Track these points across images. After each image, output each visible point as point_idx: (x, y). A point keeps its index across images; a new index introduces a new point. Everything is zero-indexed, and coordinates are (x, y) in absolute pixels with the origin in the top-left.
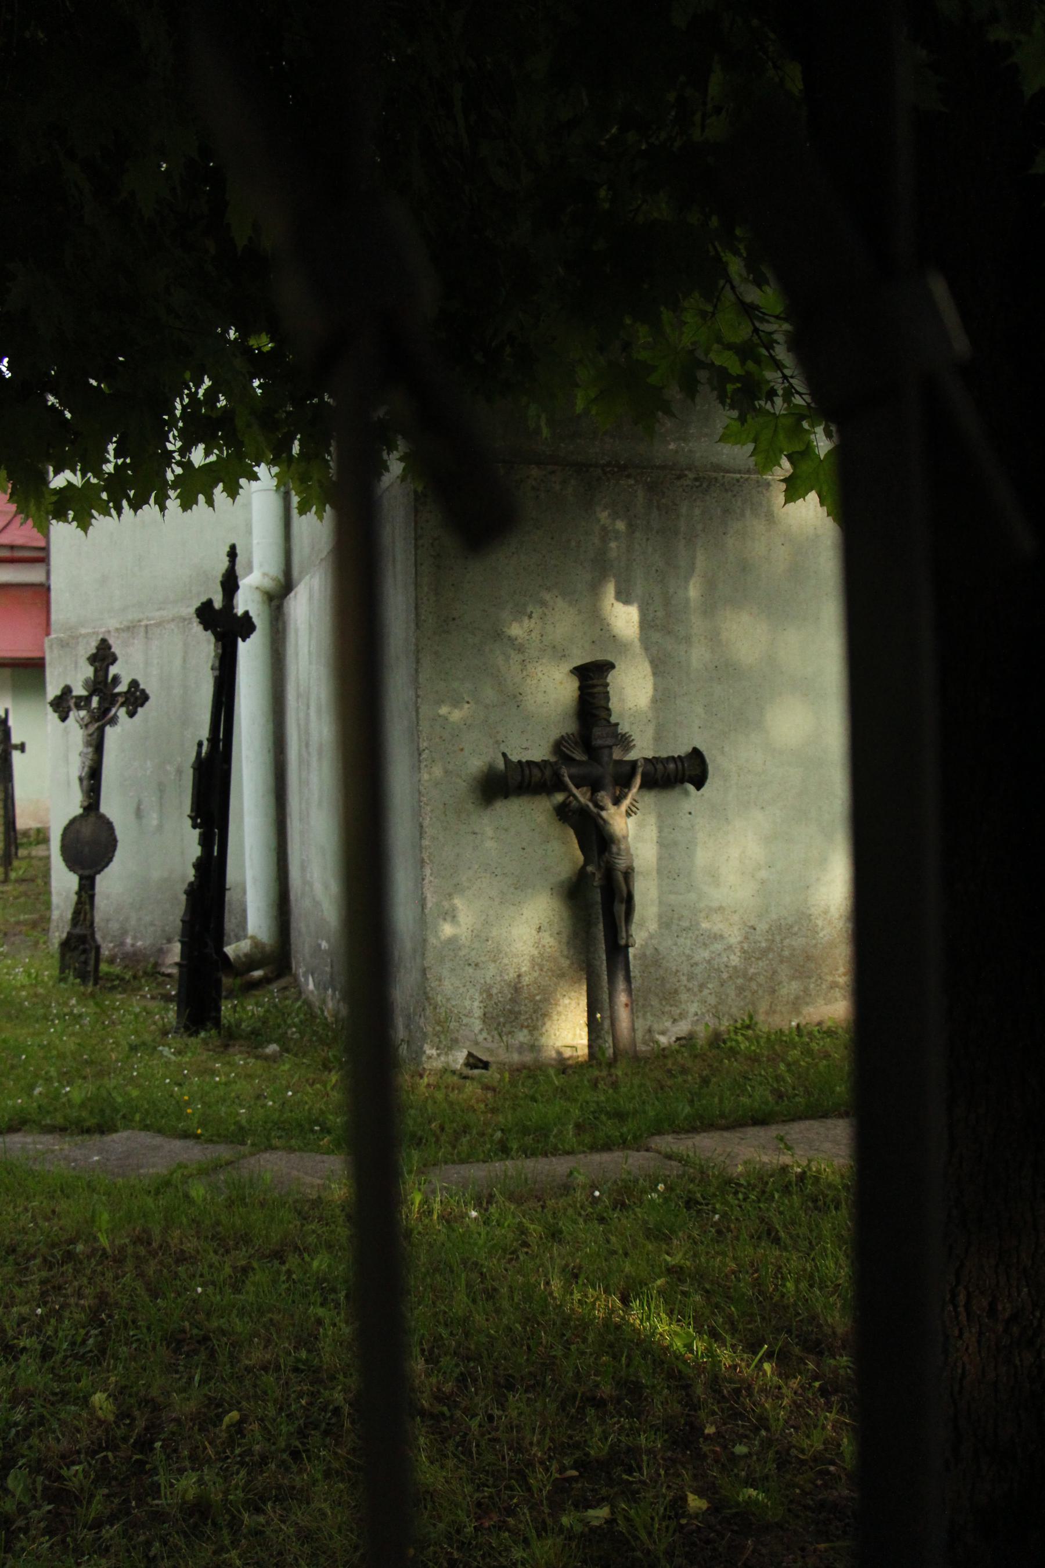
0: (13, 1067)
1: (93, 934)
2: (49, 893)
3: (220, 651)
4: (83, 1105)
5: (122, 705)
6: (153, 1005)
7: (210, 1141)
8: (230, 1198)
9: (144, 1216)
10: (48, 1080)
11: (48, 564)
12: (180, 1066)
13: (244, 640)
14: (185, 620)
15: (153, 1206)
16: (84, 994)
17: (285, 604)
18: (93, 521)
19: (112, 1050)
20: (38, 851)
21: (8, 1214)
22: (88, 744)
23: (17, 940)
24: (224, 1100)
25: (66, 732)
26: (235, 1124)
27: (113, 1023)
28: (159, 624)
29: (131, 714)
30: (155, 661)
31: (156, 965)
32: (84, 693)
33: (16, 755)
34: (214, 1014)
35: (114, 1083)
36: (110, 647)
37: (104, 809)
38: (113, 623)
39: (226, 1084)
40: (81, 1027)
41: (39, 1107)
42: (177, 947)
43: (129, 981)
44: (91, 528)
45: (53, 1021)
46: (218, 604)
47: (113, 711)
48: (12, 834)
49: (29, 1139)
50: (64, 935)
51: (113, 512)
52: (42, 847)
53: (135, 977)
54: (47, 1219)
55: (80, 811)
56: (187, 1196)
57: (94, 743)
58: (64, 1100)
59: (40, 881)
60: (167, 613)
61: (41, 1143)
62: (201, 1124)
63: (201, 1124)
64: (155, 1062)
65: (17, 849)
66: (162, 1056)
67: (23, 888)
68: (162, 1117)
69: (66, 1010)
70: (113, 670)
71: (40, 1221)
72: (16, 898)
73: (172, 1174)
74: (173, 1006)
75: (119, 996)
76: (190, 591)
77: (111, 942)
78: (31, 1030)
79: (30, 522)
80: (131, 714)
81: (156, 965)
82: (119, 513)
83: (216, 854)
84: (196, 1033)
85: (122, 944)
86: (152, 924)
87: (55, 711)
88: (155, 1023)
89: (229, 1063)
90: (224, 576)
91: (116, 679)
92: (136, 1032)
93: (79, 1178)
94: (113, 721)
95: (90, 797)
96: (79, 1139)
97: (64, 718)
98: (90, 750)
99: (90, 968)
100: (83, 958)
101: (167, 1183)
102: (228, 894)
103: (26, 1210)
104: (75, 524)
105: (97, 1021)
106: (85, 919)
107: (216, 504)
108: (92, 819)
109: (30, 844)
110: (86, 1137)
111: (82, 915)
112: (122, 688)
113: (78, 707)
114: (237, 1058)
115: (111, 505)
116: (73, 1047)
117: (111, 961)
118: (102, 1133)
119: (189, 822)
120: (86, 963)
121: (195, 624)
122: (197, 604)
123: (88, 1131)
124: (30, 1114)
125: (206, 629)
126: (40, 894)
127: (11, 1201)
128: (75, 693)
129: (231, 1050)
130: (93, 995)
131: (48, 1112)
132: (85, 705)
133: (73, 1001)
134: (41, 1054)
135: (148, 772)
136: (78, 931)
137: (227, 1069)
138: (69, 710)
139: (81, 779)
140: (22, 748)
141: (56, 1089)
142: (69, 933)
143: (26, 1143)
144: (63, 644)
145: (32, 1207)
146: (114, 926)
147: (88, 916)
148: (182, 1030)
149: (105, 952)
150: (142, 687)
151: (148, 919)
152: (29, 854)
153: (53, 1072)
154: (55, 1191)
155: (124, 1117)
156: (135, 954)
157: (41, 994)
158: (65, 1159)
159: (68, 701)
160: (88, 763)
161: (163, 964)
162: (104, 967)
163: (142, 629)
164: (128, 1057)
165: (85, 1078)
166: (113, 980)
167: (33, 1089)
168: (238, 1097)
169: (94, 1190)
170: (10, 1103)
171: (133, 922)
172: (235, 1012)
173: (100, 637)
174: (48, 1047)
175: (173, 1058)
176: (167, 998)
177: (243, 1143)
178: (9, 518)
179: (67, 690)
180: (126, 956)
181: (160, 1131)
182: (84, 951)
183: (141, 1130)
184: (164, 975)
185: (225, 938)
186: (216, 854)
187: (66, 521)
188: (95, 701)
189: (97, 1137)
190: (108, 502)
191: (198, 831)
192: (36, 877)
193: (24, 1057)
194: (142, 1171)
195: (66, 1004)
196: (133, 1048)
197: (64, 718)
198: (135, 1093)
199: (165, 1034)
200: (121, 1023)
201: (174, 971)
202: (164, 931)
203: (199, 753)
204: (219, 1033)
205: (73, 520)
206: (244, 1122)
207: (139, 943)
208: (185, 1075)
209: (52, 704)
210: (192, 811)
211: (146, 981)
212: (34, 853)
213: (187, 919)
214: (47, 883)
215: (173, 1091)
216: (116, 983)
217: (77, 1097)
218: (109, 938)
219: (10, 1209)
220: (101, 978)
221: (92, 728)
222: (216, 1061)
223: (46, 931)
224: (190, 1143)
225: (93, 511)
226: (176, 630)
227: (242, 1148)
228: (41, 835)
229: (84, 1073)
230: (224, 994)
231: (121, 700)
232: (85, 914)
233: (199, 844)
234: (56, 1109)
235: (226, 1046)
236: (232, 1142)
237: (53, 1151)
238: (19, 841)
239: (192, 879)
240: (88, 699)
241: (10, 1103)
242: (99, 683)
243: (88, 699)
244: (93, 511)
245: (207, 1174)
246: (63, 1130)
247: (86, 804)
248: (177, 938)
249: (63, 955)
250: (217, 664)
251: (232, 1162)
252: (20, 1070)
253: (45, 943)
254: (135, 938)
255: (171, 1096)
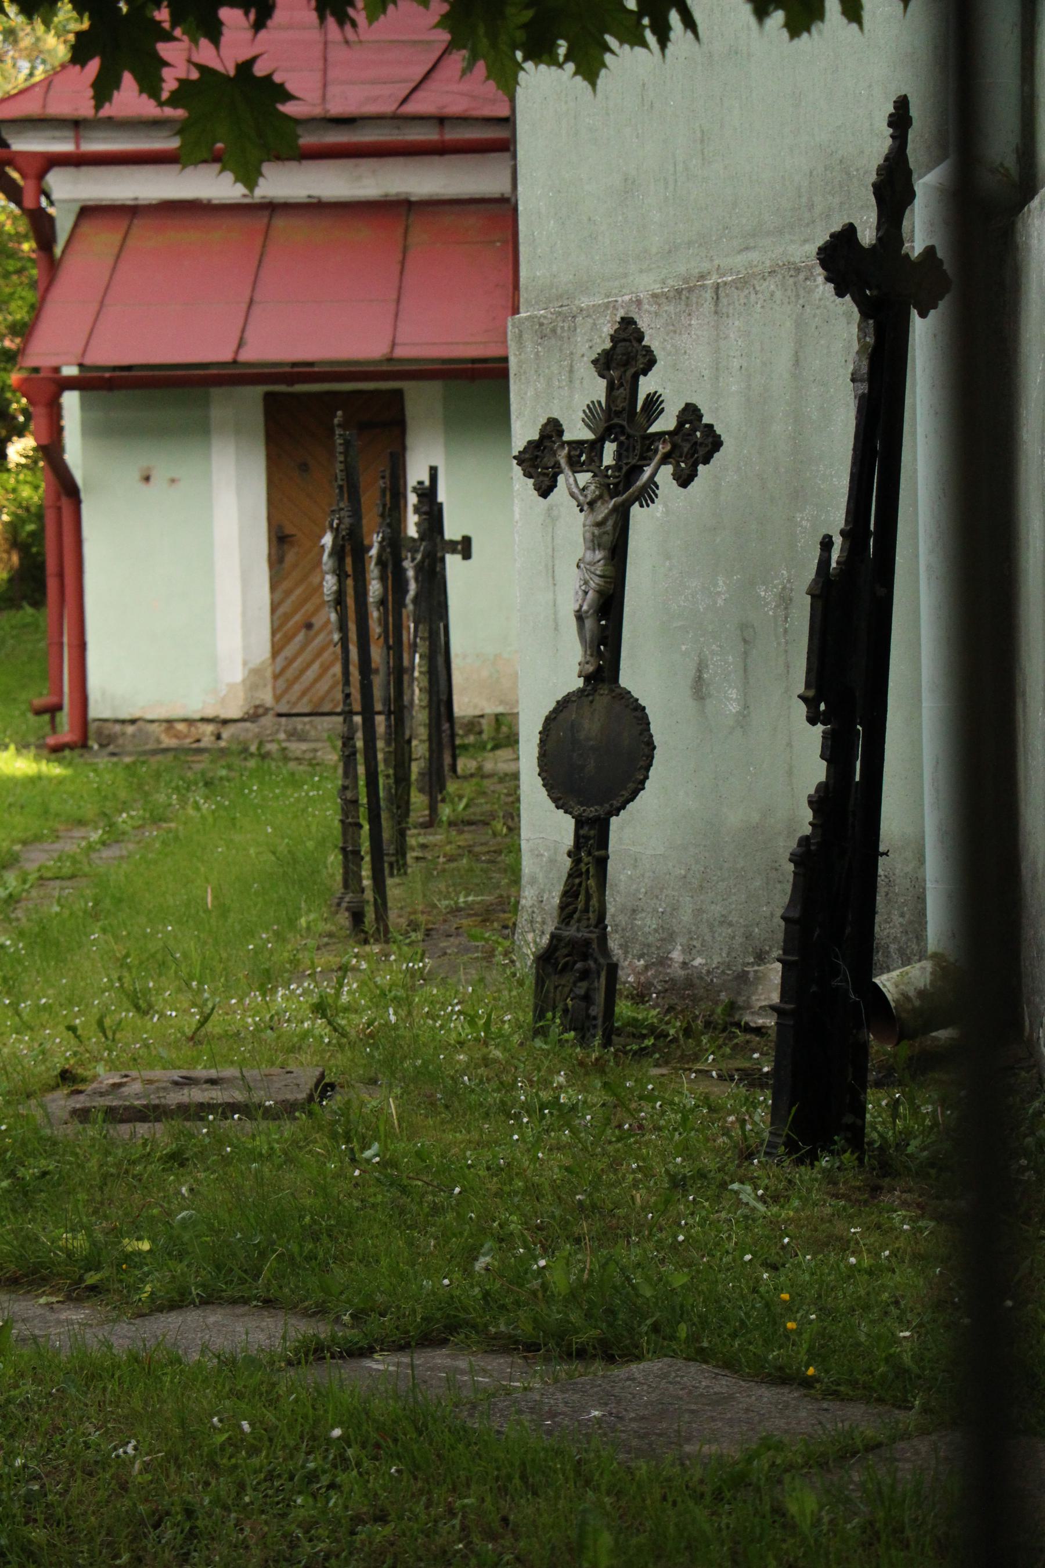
0: (436, 1210)
1: (603, 938)
2: (516, 850)
3: (870, 340)
4: (573, 1297)
5: (665, 460)
6: (727, 1093)
7: (833, 1394)
8: (871, 1523)
9: (688, 1547)
10: (504, 1239)
11: (514, 157)
12: (773, 1223)
13: (923, 315)
14: (798, 270)
15: (706, 1527)
16: (581, 1064)
17: (1019, 225)
18: (608, 57)
19: (635, 1184)
20: (495, 762)
21: (416, 1518)
22: (594, 543)
23: (450, 945)
24: (867, 1308)
25: (551, 517)
26: (887, 1360)
27: (641, 1127)
28: (742, 283)
29: (684, 480)
30: (736, 363)
31: (732, 1007)
32: (588, 435)
33: (453, 562)
34: (849, 1119)
35: (635, 1255)
36: (640, 336)
37: (625, 680)
38: (647, 283)
39: (870, 1272)
40: (574, 1132)
41: (486, 1295)
42: (775, 972)
43: (675, 1040)
44: (603, 72)
45: (517, 1117)
46: (867, 236)
47: (648, 471)
48: (446, 726)
49: (462, 1364)
50: (545, 940)
51: (649, 36)
52: (504, 753)
53: (688, 1032)
54: (491, 1536)
55: (580, 683)
56: (779, 1511)
57: (607, 539)
58: (536, 1284)
59: (499, 826)
60: (759, 258)
61: (485, 1372)
62: (813, 1357)
63: (813, 1357)
64: (723, 1215)
65: (454, 758)
66: (739, 1203)
67: (465, 839)
68: (734, 1335)
69: (545, 1095)
70: (647, 385)
71: (476, 1539)
72: (451, 859)
73: (749, 1460)
74: (764, 1097)
75: (655, 1071)
76: (811, 207)
77: (641, 956)
78: (475, 1136)
79: (481, 66)
80: (684, 480)
81: (732, 1007)
82: (663, 40)
83: (857, 779)
84: (813, 1158)
85: (663, 961)
86: (724, 921)
87: (528, 475)
88: (726, 1132)
89: (878, 1226)
90: (880, 170)
91: (654, 404)
92: (686, 1150)
93: (558, 1453)
94: (647, 494)
95: (600, 655)
96: (562, 1369)
97: (545, 491)
98: (599, 555)
99: (597, 1010)
100: (581, 989)
101: (740, 1480)
102: (883, 866)
103: (451, 1512)
104: (570, 67)
105: (608, 1121)
106: (586, 910)
107: (866, 16)
108: (602, 699)
109: (483, 748)
110: (578, 1366)
111: (582, 897)
112: (666, 422)
113: (576, 466)
114: (897, 1216)
115: (646, 21)
116: (557, 1175)
117: (640, 997)
118: (611, 1359)
119: (802, 709)
120: (587, 998)
121: (820, 279)
122: (822, 238)
123: (581, 1354)
124: (466, 1310)
125: (840, 293)
126: (499, 852)
127: (421, 1492)
128: (567, 437)
129: (885, 1199)
130: (600, 1066)
131: (503, 1307)
132: (591, 460)
133: (561, 1079)
134: (493, 1185)
135: (720, 602)
136: (571, 932)
137: (873, 1239)
138: (557, 471)
139: (580, 617)
140: (464, 547)
141: (520, 1259)
142: (553, 936)
143: (457, 1370)
144: (545, 332)
145: (464, 1506)
146: (648, 923)
147: (594, 902)
148: (782, 1149)
149: (628, 977)
150: (705, 420)
151: (717, 910)
152: (480, 768)
153: (515, 1224)
154: (510, 1478)
155: (656, 1328)
156: (689, 983)
157: (496, 1061)
158: (532, 1410)
159: (554, 454)
160: (595, 582)
161: (748, 1006)
162: (624, 1008)
163: (709, 295)
164: (667, 1202)
165: (578, 1241)
166: (644, 1037)
167: (476, 1259)
168: (897, 1303)
169: (588, 1483)
170: (427, 1284)
171: (686, 916)
172: (895, 1115)
173: (621, 313)
174: (507, 1172)
175: (761, 1207)
176: (752, 1079)
177: (905, 1405)
178: (437, 54)
179: (552, 429)
180: (672, 986)
181: (730, 1365)
182: (585, 975)
183: (688, 1359)
184: (747, 1029)
185: (878, 957)
186: (857, 779)
187: (553, 61)
188: (609, 453)
189: (598, 1367)
190: (640, 15)
191: (820, 728)
192: (493, 816)
193: (457, 1190)
194: (688, 1448)
195: (546, 1083)
196: (678, 1183)
197: (545, 491)
198: (680, 1280)
199: (748, 1155)
200: (658, 1128)
201: (769, 1021)
202: (748, 937)
203: (824, 562)
204: (860, 1160)
205: (568, 58)
206: (907, 1359)
207: (698, 961)
208: (783, 1247)
209: (520, 460)
210: (808, 686)
211: (712, 1040)
212: (488, 766)
213: (795, 914)
214: (514, 830)
215: (758, 1280)
216: (649, 1042)
217: (560, 1281)
218: (636, 949)
219: (419, 1509)
220: (619, 1032)
221: (603, 510)
222: (851, 1220)
223: (509, 929)
224: (789, 1395)
225: (608, 38)
226: (778, 294)
227: (900, 1415)
228: (504, 729)
229: (576, 1230)
230: (872, 1076)
231: (663, 449)
232: (588, 897)
233: (822, 757)
234: (517, 1303)
235: (875, 1190)
236: (880, 1400)
237: (508, 1392)
238: (458, 742)
239: (808, 830)
240: (595, 447)
241: (427, 1284)
242: (618, 414)
243: (595, 447)
244: (608, 38)
245: (823, 1466)
246: (532, 1347)
247: (590, 668)
248: (777, 953)
249: (540, 982)
250: (864, 370)
251: (879, 1445)
252: (450, 1216)
253: (506, 954)
254: (689, 949)
255: (755, 1290)
